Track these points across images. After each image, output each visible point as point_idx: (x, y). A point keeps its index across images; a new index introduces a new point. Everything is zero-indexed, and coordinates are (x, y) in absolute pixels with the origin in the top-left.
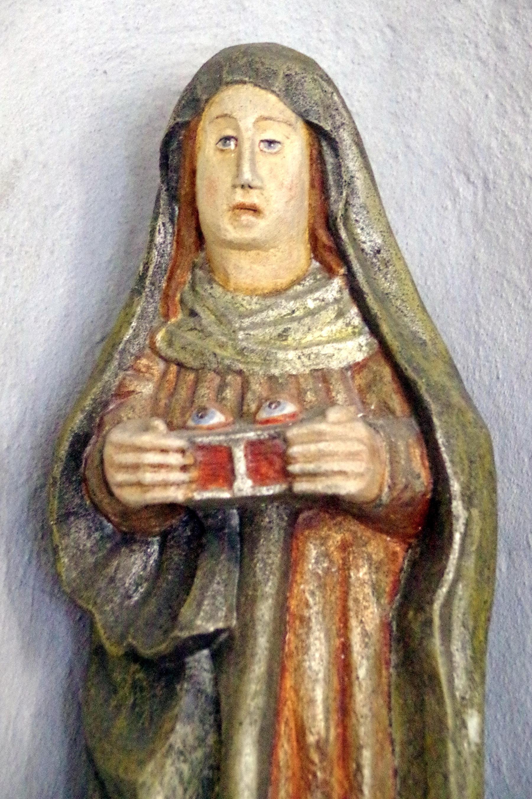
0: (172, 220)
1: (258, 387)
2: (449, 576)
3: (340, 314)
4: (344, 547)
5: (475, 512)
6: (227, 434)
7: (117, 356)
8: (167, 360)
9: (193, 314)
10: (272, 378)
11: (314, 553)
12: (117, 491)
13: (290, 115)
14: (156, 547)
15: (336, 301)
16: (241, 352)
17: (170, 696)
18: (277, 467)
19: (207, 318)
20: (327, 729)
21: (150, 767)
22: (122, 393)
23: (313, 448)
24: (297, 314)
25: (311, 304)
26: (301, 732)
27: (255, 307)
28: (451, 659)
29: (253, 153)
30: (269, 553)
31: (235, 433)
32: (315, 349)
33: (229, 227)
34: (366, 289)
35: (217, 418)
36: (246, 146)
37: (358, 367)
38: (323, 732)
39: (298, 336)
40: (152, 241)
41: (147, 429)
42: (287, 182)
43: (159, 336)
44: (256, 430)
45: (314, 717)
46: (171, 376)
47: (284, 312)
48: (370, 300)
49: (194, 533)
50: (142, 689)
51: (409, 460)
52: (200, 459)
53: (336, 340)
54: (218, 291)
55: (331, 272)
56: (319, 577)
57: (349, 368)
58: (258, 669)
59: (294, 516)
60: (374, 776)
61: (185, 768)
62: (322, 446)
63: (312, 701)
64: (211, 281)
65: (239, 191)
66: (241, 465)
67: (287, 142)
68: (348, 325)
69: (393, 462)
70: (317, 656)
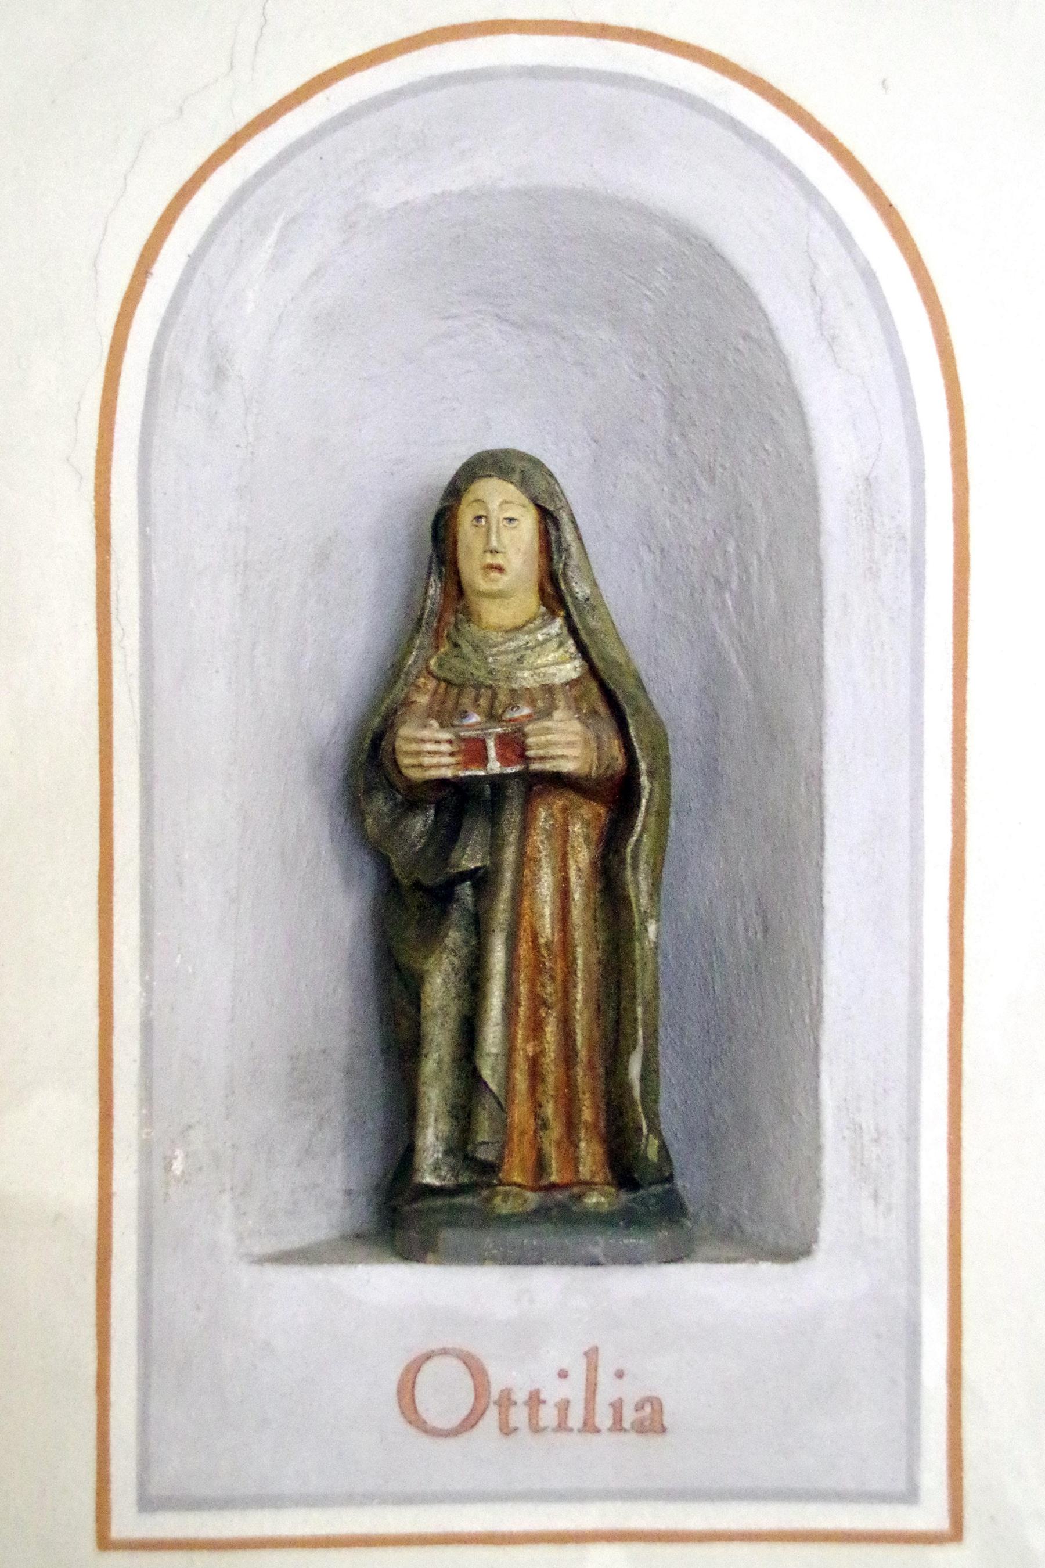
0: (440, 578)
1: (503, 697)
2: (638, 829)
3: (561, 644)
4: (564, 810)
5: (656, 785)
6: (482, 730)
7: (403, 676)
8: (438, 679)
9: (456, 645)
10: (513, 691)
11: (543, 814)
12: (404, 770)
13: (524, 500)
14: (432, 811)
15: (558, 635)
16: (490, 672)
17: (445, 913)
18: (518, 753)
19: (466, 649)
20: (553, 935)
21: (431, 960)
22: (407, 703)
23: (543, 738)
24: (530, 644)
25: (540, 637)
26: (535, 937)
27: (500, 639)
28: (638, 886)
29: (498, 527)
30: (512, 816)
31: (487, 729)
32: (543, 670)
33: (481, 582)
34: (579, 626)
35: (475, 719)
36: (494, 522)
37: (572, 683)
38: (550, 936)
39: (531, 660)
40: (426, 593)
41: (425, 726)
42: (523, 547)
43: (433, 662)
44: (502, 727)
45: (544, 926)
46: (441, 690)
47: (521, 643)
48: (582, 633)
49: (460, 802)
50: (425, 908)
51: (610, 747)
52: (463, 748)
53: (558, 664)
54: (473, 628)
55: (554, 615)
56: (547, 831)
57: (567, 683)
58: (505, 893)
59: (530, 788)
60: (585, 964)
61: (456, 962)
62: (549, 737)
63: (543, 916)
64: (469, 621)
65: (488, 555)
66: (492, 753)
67: (522, 519)
68: (566, 652)
69: (599, 748)
70: (546, 885)
